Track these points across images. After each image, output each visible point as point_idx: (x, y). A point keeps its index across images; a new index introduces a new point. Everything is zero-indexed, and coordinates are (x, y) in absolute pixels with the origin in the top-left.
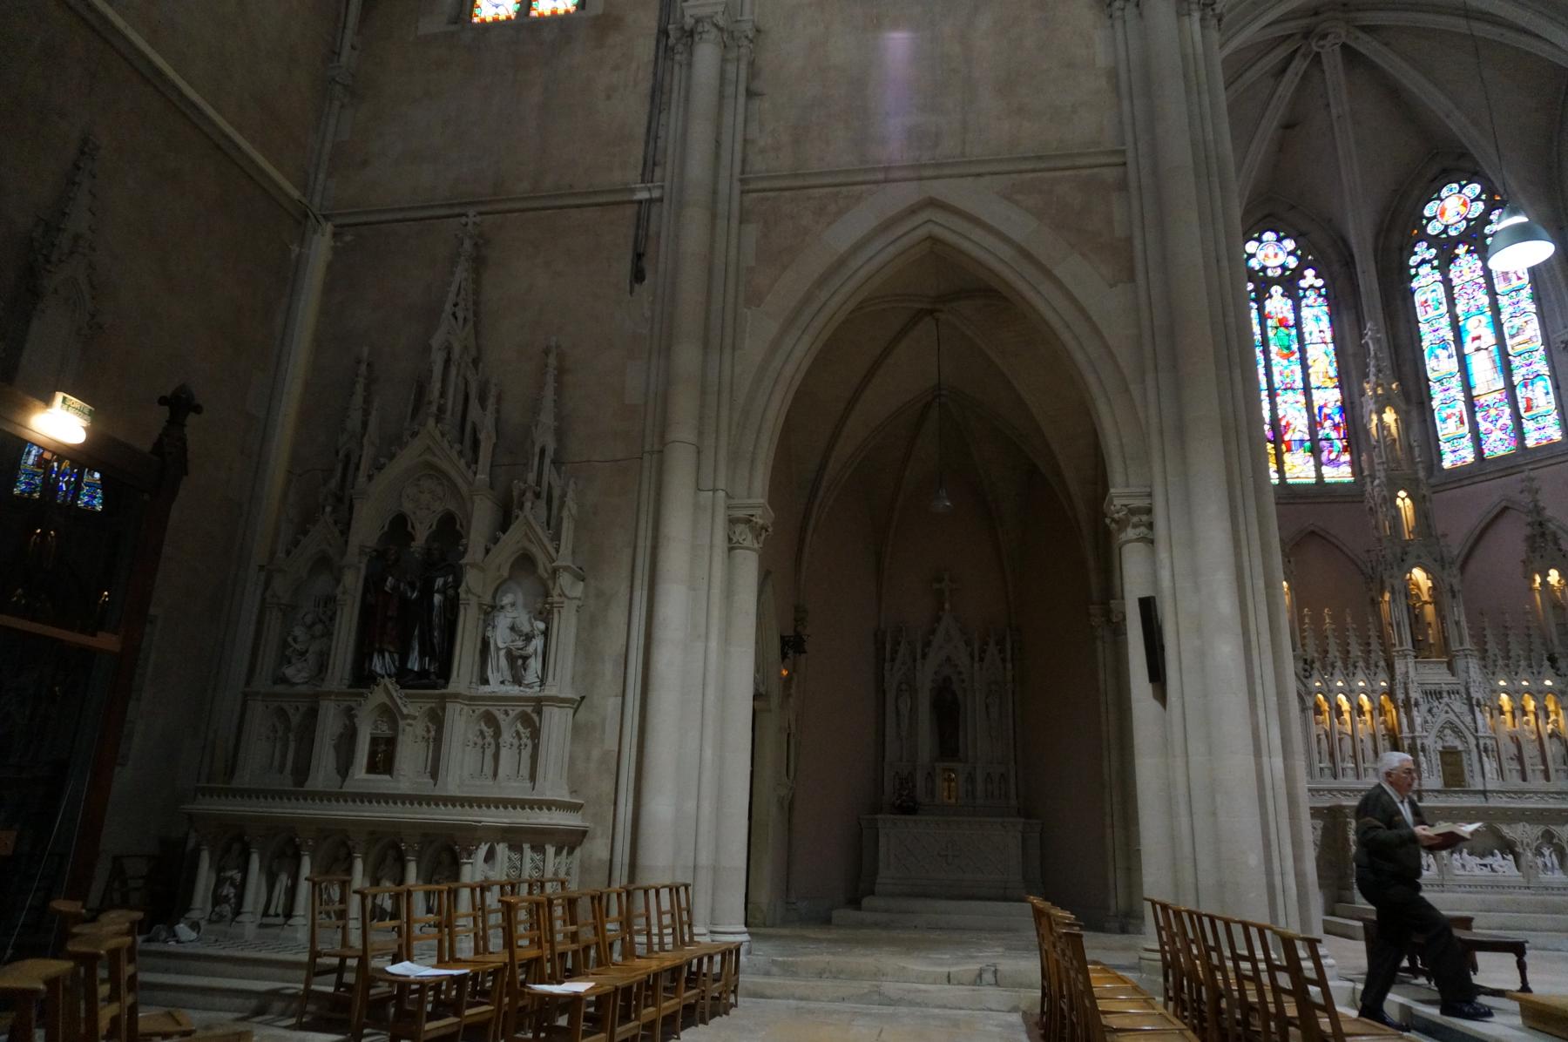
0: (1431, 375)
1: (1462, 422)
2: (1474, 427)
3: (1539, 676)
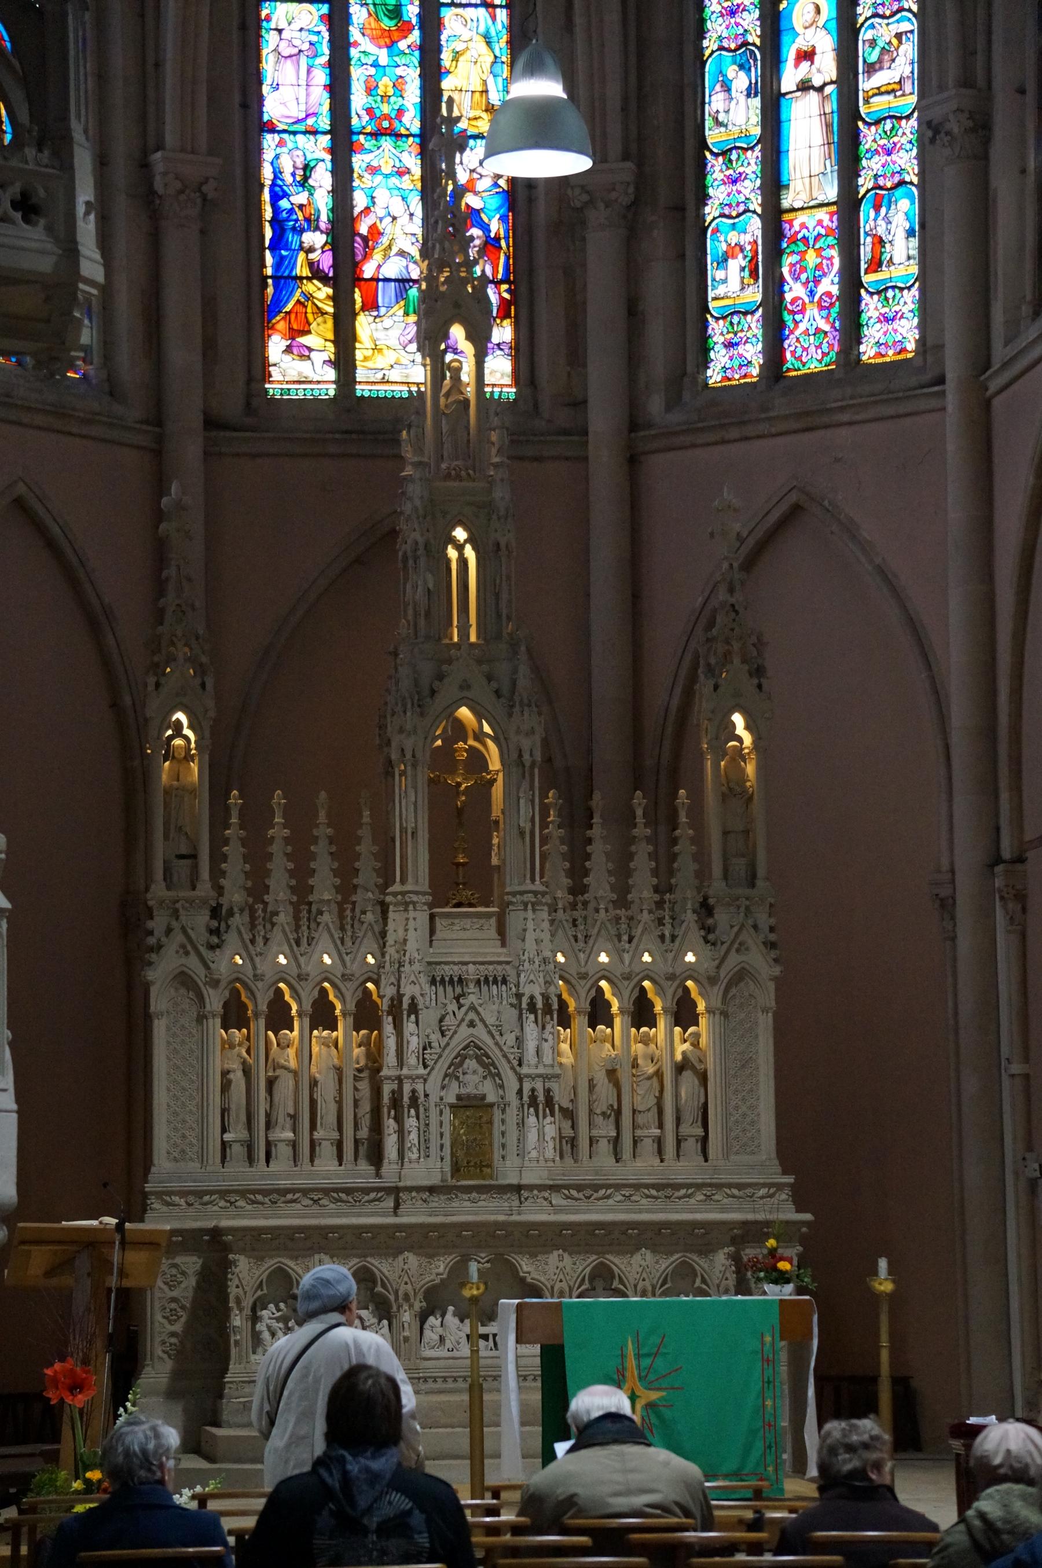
0: (714, 136)
1: (754, 274)
2: (774, 287)
3: (670, 943)
